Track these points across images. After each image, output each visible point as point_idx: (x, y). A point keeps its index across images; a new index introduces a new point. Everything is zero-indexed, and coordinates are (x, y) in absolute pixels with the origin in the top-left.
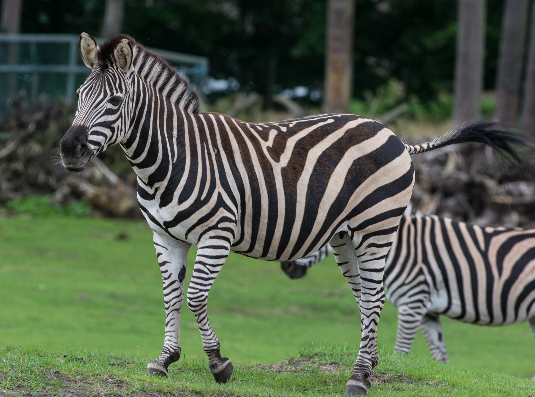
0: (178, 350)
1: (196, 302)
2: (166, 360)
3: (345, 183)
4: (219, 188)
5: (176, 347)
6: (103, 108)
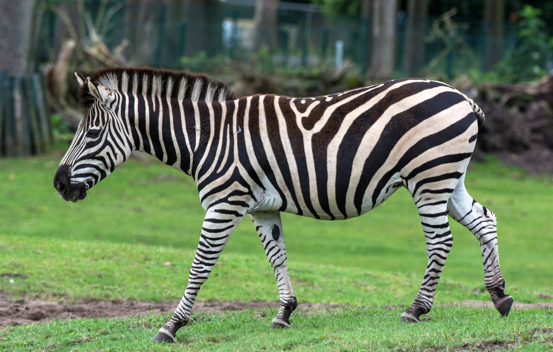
0: (291, 300)
1: (194, 271)
2: (284, 313)
3: (380, 138)
4: (237, 163)
5: (288, 297)
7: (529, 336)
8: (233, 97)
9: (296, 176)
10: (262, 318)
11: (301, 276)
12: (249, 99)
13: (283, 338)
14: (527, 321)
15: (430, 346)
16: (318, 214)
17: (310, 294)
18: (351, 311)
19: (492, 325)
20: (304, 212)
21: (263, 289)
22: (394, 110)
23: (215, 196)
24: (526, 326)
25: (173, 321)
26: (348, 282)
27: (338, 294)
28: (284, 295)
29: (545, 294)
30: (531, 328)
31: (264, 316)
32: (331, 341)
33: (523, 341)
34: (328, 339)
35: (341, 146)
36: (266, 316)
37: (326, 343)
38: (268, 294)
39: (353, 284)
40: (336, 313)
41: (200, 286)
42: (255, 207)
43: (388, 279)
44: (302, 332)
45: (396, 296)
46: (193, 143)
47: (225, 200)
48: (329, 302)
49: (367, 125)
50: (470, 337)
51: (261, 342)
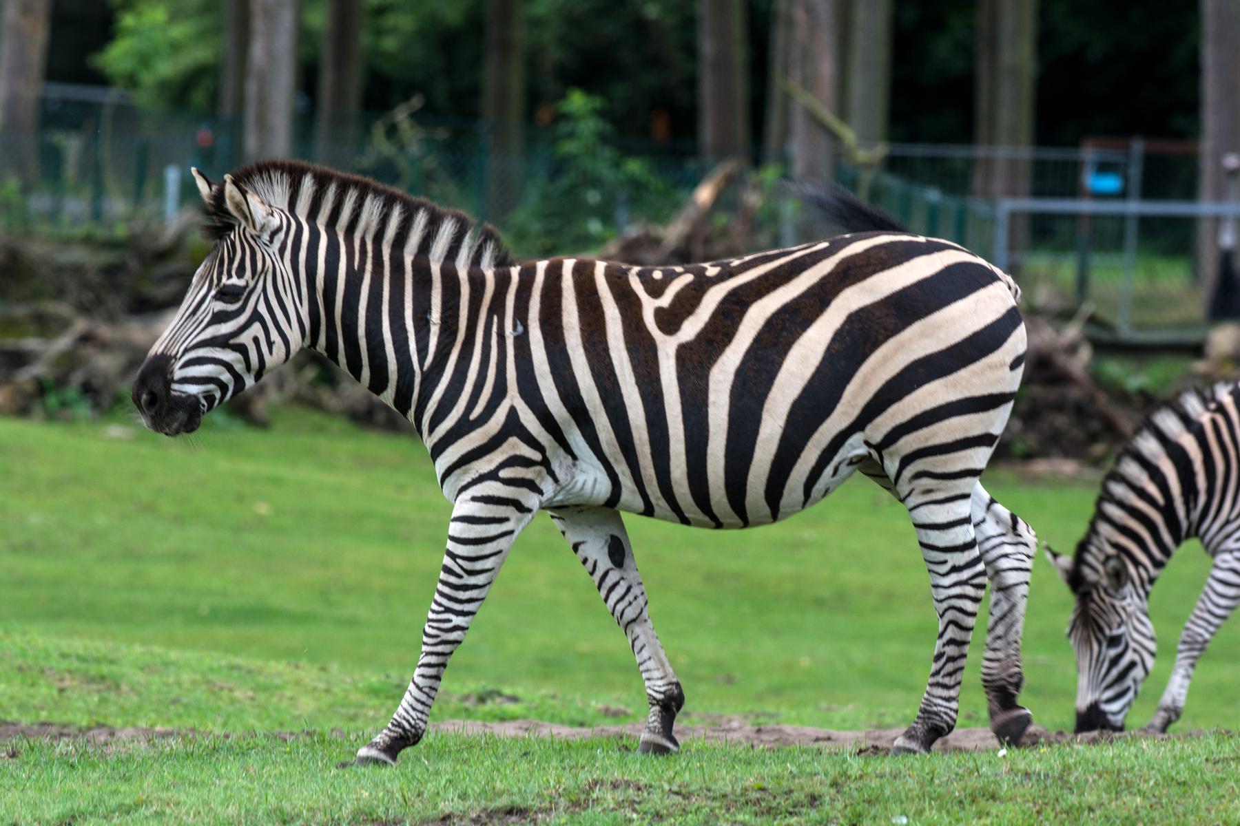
0: (671, 689)
1: (433, 628)
2: (662, 719)
4: (513, 398)
6: (206, 312)
7: (583, 797)
8: (509, 260)
9: (642, 432)
10: (10, 760)
11: (93, 670)
12: (542, 266)
13: (54, 802)
14: (577, 764)
15: (370, 818)
16: (686, 515)
17: (113, 709)
18: (201, 746)
19: (503, 773)
20: (657, 509)
21: (12, 698)
22: (853, 299)
23: (470, 469)
24: (576, 776)
25: (388, 733)
26: (194, 683)
27: (172, 707)
28: (653, 682)
29: (614, 706)
30: (587, 779)
31: (13, 755)
32: (159, 809)
33: (568, 808)
34: (152, 806)
35: (740, 373)
36: (17, 757)
37: (148, 813)
38: (22, 707)
39: (204, 687)
40: (168, 748)
41: (446, 660)
42: (555, 496)
43: (279, 675)
44: (95, 790)
45: (297, 713)
46: (423, 351)
47: (492, 476)
48: (152, 726)
49: (796, 330)
50: (456, 799)
51: (7, 812)
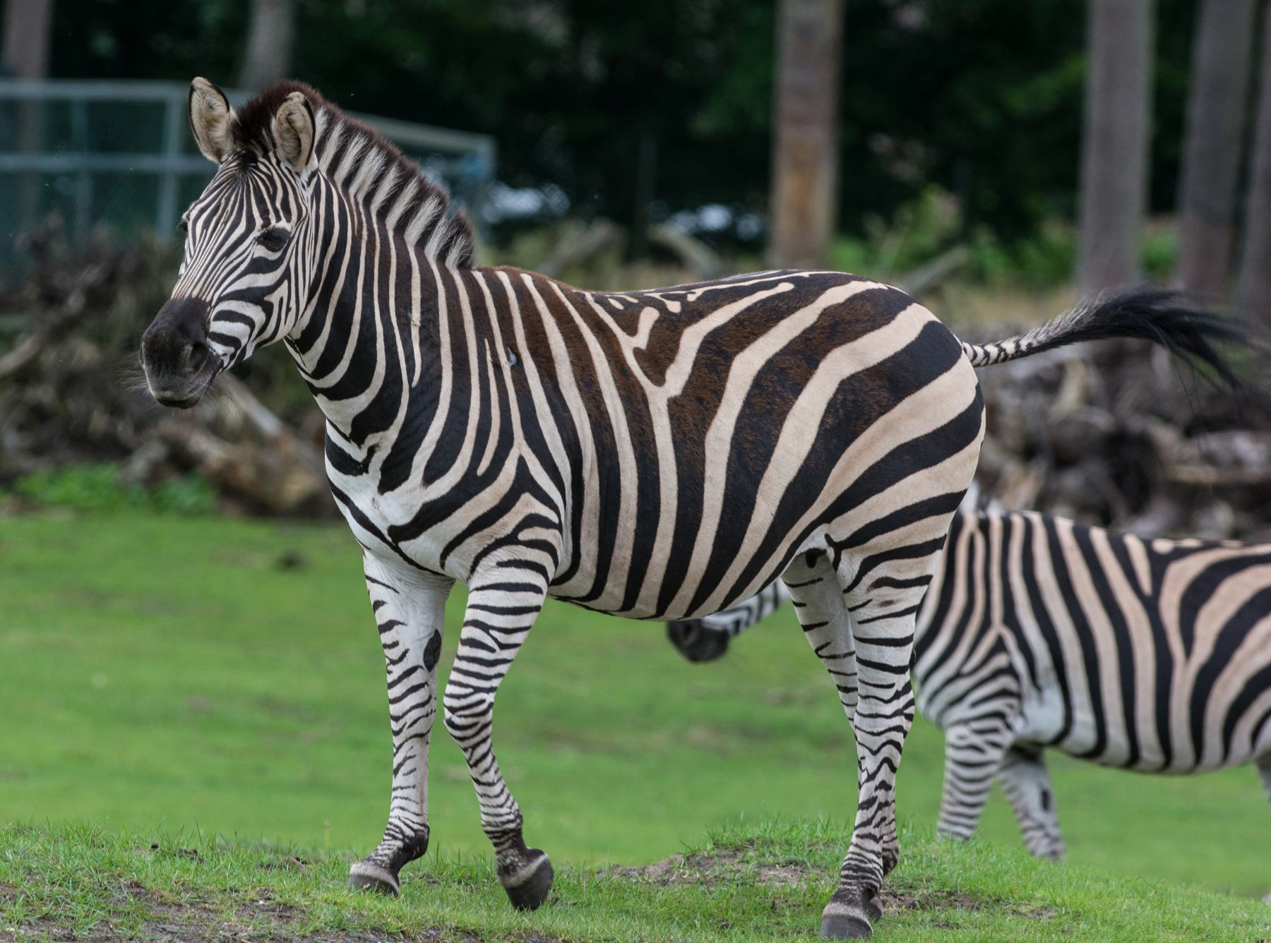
0: (423, 831)
1: (465, 716)
2: (394, 856)
3: (819, 435)
4: (520, 447)
5: (417, 823)
6: (244, 256)
